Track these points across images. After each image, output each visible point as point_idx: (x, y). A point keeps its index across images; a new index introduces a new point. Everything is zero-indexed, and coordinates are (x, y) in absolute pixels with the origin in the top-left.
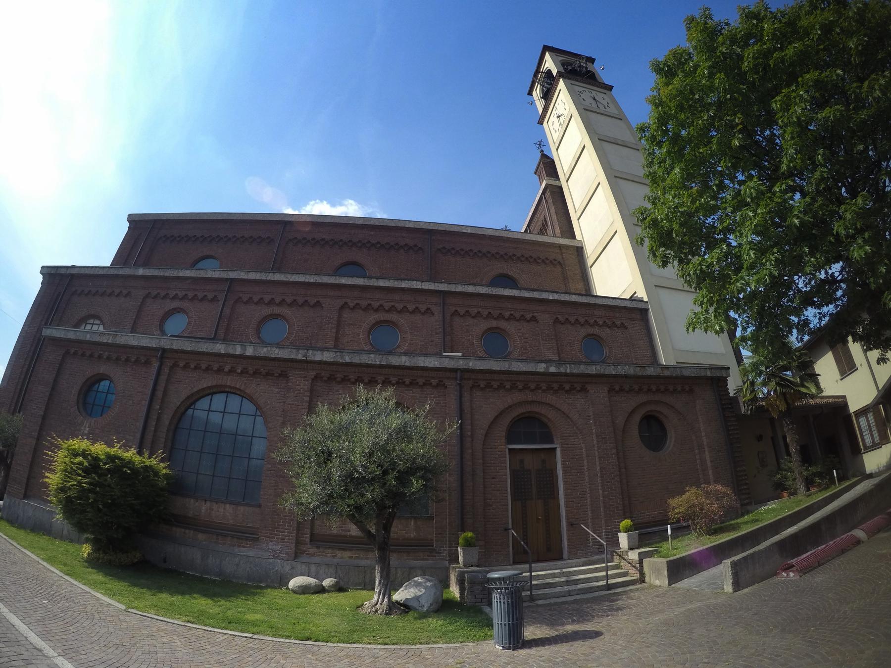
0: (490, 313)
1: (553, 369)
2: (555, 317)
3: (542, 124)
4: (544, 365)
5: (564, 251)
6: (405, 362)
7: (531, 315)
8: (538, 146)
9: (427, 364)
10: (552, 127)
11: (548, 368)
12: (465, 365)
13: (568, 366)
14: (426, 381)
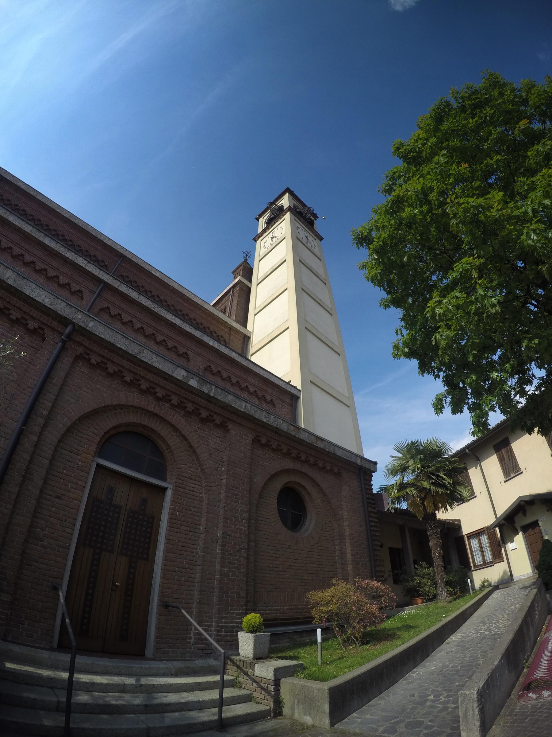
0: (142, 328)
1: (193, 383)
2: (208, 364)
3: (256, 241)
4: (184, 373)
5: (232, 333)
6: (8, 278)
7: (184, 350)
8: (245, 255)
9: (34, 295)
10: (263, 245)
11: (188, 378)
12: (83, 322)
13: (213, 387)
14: (22, 317)
